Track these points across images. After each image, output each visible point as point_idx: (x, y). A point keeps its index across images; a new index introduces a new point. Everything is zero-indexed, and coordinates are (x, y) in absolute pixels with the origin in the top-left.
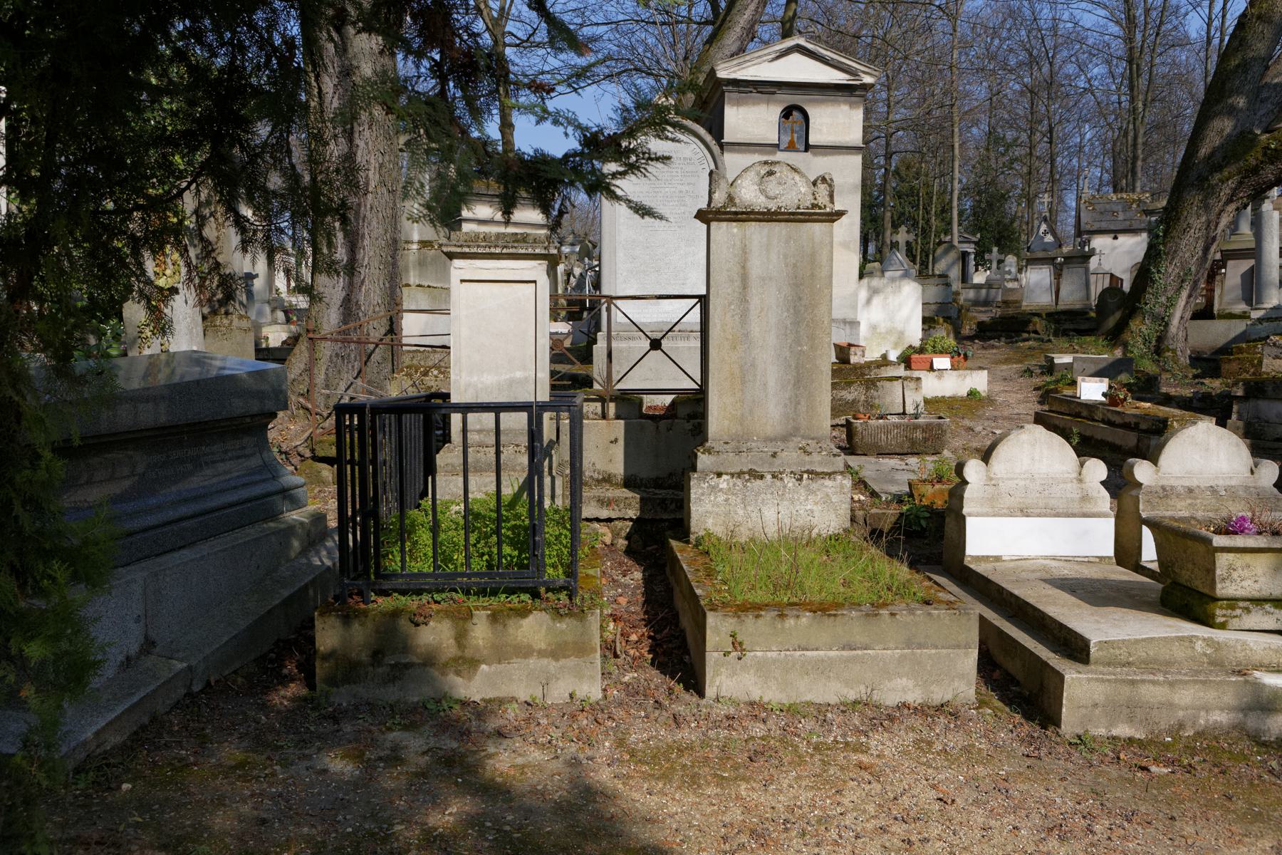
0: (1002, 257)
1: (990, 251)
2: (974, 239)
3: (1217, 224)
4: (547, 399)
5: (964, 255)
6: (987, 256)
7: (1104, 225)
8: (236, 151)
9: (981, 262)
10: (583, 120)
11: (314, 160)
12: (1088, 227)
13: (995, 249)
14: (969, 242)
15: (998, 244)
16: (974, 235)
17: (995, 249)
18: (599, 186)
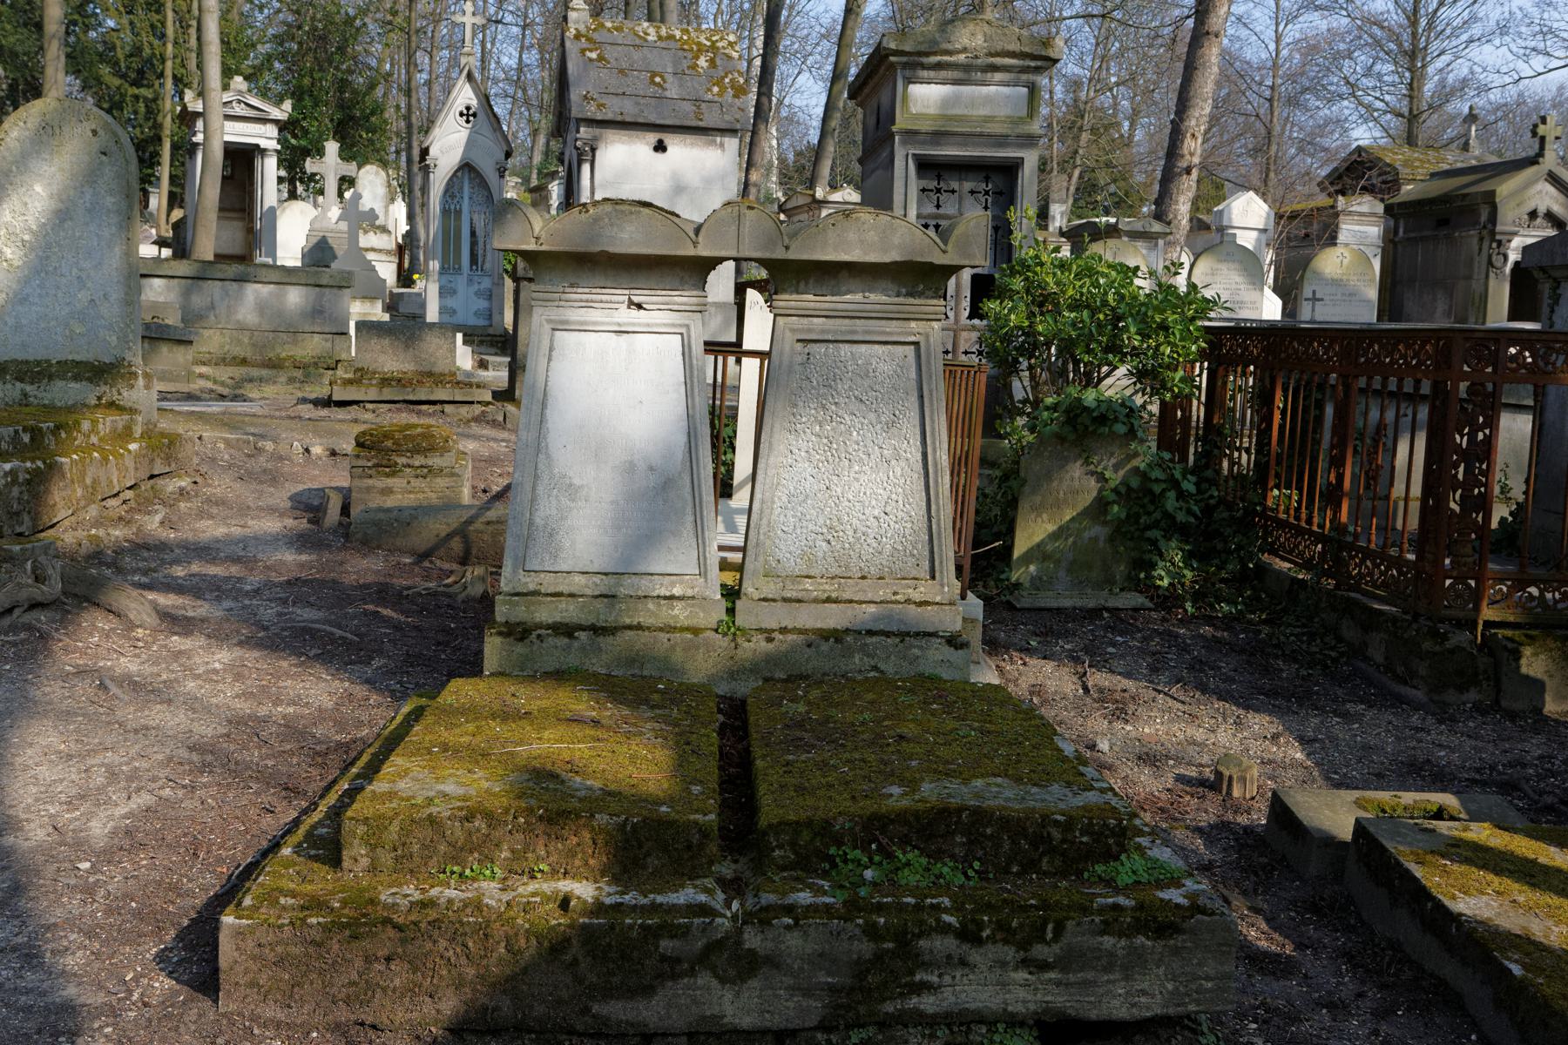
0: (350, 169)
1: (321, 152)
2: (276, 113)
3: (834, 162)
4: (1278, 317)
5: (241, 159)
6: (310, 166)
7: (629, 110)
8: (1409, 456)
9: (297, 181)
10: (745, 585)
11: (293, 894)
12: (591, 111)
13: (332, 147)
14: (264, 121)
15: (342, 132)
16: (278, 102)
17: (332, 147)
18: (354, 103)
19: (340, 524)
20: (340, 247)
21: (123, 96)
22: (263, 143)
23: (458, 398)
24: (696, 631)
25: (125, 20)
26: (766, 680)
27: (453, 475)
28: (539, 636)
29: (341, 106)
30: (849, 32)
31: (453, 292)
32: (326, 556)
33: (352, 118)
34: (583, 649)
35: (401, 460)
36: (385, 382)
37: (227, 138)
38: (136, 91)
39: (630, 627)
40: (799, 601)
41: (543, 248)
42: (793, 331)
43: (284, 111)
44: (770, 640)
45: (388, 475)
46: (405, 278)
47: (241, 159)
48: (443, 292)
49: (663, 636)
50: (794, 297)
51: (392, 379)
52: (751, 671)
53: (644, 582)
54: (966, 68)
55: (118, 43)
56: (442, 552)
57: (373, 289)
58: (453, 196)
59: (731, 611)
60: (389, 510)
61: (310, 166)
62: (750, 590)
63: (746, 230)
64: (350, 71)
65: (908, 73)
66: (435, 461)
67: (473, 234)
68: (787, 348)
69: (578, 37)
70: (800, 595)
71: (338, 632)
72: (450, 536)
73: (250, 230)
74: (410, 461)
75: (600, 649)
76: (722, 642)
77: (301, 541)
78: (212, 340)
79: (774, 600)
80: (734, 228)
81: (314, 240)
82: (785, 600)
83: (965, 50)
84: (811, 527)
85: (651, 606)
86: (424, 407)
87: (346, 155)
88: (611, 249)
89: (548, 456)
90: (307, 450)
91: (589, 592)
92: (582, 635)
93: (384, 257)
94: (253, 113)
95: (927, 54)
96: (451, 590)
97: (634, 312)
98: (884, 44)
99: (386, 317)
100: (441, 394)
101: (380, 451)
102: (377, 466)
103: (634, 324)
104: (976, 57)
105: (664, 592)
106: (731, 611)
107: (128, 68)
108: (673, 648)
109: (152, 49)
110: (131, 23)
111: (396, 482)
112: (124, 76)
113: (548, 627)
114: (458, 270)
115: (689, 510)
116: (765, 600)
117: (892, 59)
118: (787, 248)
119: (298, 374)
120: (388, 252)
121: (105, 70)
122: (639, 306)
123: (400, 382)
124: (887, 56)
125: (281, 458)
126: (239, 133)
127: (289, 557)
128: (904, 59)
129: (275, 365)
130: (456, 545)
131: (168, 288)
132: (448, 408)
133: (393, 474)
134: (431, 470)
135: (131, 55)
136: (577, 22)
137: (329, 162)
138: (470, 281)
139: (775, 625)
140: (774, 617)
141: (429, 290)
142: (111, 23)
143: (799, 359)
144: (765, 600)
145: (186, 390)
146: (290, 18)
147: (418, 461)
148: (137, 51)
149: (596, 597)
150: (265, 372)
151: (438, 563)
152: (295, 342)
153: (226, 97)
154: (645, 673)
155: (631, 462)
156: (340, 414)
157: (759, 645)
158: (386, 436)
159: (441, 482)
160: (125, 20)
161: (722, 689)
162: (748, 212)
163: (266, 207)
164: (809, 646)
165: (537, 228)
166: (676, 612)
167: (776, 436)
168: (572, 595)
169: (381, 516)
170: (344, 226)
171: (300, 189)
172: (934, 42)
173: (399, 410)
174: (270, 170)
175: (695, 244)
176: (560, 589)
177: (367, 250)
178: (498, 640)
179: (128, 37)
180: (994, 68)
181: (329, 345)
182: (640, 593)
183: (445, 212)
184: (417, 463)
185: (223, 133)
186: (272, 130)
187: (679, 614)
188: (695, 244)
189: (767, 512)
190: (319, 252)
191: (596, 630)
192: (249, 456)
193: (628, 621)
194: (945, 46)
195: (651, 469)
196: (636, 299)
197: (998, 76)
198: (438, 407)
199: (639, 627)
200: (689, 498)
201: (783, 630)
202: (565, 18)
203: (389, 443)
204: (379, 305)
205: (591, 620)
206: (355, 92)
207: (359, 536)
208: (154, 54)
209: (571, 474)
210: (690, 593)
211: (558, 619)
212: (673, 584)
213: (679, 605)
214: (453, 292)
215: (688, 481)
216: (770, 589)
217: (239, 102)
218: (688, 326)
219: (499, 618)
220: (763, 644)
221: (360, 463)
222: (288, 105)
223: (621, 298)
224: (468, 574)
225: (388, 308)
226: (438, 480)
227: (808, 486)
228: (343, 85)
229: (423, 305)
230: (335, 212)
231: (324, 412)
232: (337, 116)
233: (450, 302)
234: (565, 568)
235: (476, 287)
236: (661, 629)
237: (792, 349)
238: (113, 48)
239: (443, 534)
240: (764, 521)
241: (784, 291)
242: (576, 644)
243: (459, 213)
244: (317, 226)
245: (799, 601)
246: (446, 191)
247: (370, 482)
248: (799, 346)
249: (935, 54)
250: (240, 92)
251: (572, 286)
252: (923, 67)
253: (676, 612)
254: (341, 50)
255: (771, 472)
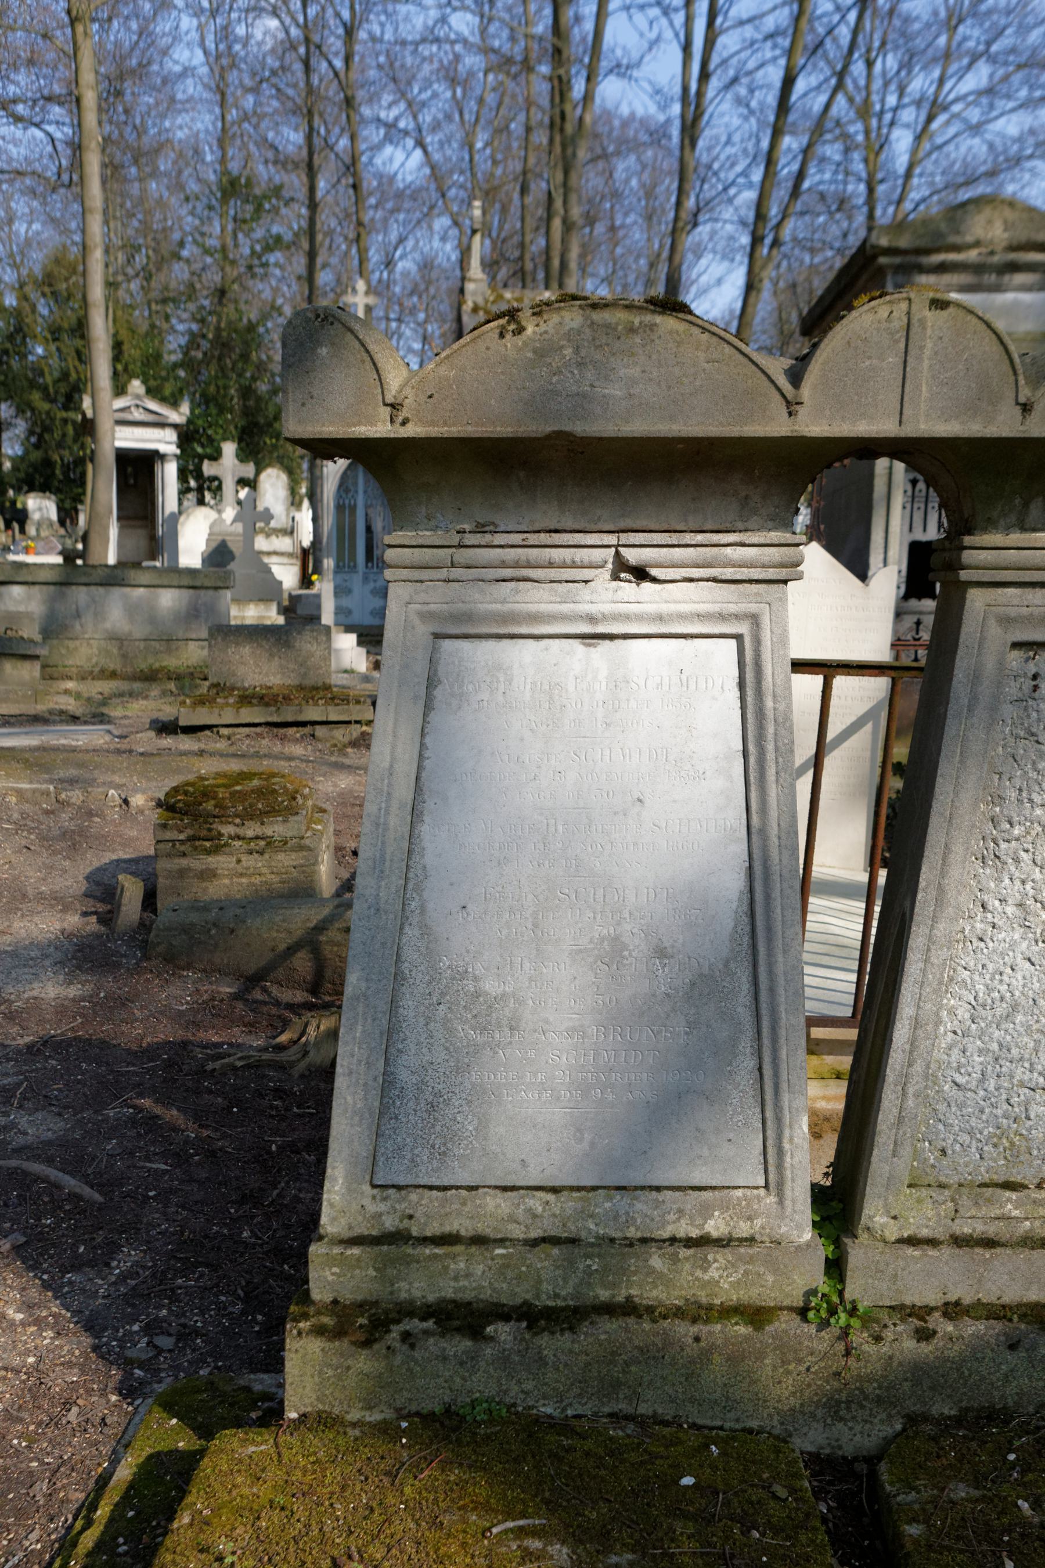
6: (208, 469)
9: (200, 487)
13: (229, 449)
14: (162, 425)
16: (174, 404)
17: (229, 449)
19: (142, 924)
20: (236, 547)
21: (53, 419)
22: (163, 448)
23: (333, 717)
24: (757, 1315)
25: (53, 347)
26: (912, 1420)
27: (301, 848)
28: (406, 1336)
29: (246, 412)
30: (749, 310)
31: (349, 591)
32: (109, 983)
33: (256, 424)
34: (504, 1361)
35: (227, 830)
36: (247, 698)
37: (119, 444)
38: (64, 414)
39: (609, 1309)
40: (989, 1243)
41: (411, 431)
42: (1006, 621)
43: (179, 415)
44: (924, 1335)
45: (208, 852)
46: (306, 581)
47: (136, 468)
48: (340, 592)
49: (684, 1330)
50: (1016, 538)
51: (253, 696)
52: (879, 1400)
53: (642, 1205)
54: (978, 269)
55: (46, 370)
56: (280, 973)
57: (267, 589)
58: (347, 491)
59: (836, 1267)
60: (206, 908)
61: (208, 469)
62: (880, 1220)
63: (923, 366)
64: (254, 379)
65: (900, 278)
66: (276, 829)
67: (369, 529)
68: (990, 664)
69: (475, 309)
70: (991, 1230)
71: (70, 1183)
72: (292, 950)
73: (153, 538)
74: (240, 831)
75: (542, 1361)
76: (816, 1341)
77: (82, 956)
78: (85, 649)
79: (932, 1242)
80: (893, 360)
81: (214, 545)
82: (959, 1241)
83: (977, 244)
84: (1020, 1074)
85: (656, 1262)
86: (291, 731)
87: (243, 456)
88: (581, 428)
89: (426, 930)
90: (126, 801)
91: (517, 1232)
92: (503, 1331)
93: (285, 560)
94: (150, 418)
95: (928, 252)
96: (283, 1057)
97: (628, 589)
98: (874, 239)
99: (281, 620)
100: (313, 713)
101: (196, 817)
102: (192, 839)
103: (627, 618)
104: (992, 253)
105: (685, 1229)
106: (836, 1267)
107: (56, 392)
108: (706, 1355)
109: (78, 372)
110: (58, 349)
111: (221, 862)
112: (53, 401)
113: (428, 1311)
114: (354, 568)
115: (746, 1044)
116: (912, 1241)
117: (883, 260)
118: (1026, 408)
119: (172, 686)
120: (290, 555)
121: (36, 397)
122: (641, 574)
123: (263, 698)
124: (874, 257)
125: (90, 814)
126: (129, 439)
127: (52, 989)
128: (897, 260)
129: (150, 677)
130: (302, 963)
131: (29, 598)
132: (320, 731)
133: (216, 850)
134: (269, 841)
135: (59, 380)
136: (474, 293)
137: (228, 462)
138: (366, 579)
139: (933, 1298)
140: (933, 1278)
141: (325, 588)
142: (40, 351)
143: (1012, 689)
144: (912, 1241)
145: (32, 712)
146: (194, 327)
147: (251, 830)
148: (65, 375)
149: (534, 1243)
150: (137, 686)
151: (275, 990)
152: (169, 651)
153: (120, 403)
154: (644, 1409)
155: (616, 938)
156: (186, 743)
157: (902, 1343)
158: (207, 794)
159: (285, 860)
160: (53, 347)
161: (811, 1439)
162: (932, 317)
163: (167, 512)
164: (1013, 1347)
165: (395, 380)
166: (713, 1273)
167: (955, 872)
168: (479, 1241)
169: (194, 917)
170: (239, 527)
171: (208, 496)
172: (939, 235)
173: (260, 735)
174: (170, 472)
175: (792, 406)
176: (453, 1226)
177: (269, 554)
178: (315, 1346)
179: (54, 362)
180: (1014, 267)
181: (205, 652)
182: (632, 1233)
183: (340, 508)
184: (250, 833)
185: (114, 439)
186: (171, 435)
187: (722, 1278)
188: (792, 406)
189: (923, 1044)
190: (219, 555)
191: (534, 1317)
192: (47, 812)
193: (604, 1295)
194: (953, 239)
195: (661, 953)
196: (632, 556)
197: (1020, 278)
198: (308, 730)
199: (629, 1309)
200: (745, 1015)
201: (953, 1310)
202: (462, 291)
203: (209, 806)
204: (274, 608)
205: (523, 1293)
206: (259, 399)
207: (160, 949)
208: (79, 379)
209: (479, 970)
210: (744, 1229)
211: (449, 1294)
212: (706, 1210)
213: (719, 1258)
214: (349, 591)
215: (746, 986)
216: (925, 1216)
217: (137, 406)
218: (754, 619)
219: (319, 1293)
220: (909, 1344)
221: (169, 835)
222: (185, 408)
223: (597, 555)
224: (311, 1031)
225: (284, 611)
226: (281, 856)
227: (1018, 982)
228: (247, 392)
229: (319, 607)
230: (230, 513)
231: (168, 741)
232: (242, 423)
233: (346, 602)
234: (464, 1178)
235: (372, 585)
236: (678, 1313)
237: (1001, 663)
238: (42, 374)
239: (282, 947)
240: (918, 1067)
241: (990, 525)
242: (489, 1351)
243: (353, 509)
244: (216, 529)
245: (989, 1243)
246: (340, 486)
247: (184, 862)
248: (1015, 658)
249: (938, 250)
250: (138, 397)
251: (480, 529)
252: (922, 269)
253: (713, 1273)
254: (245, 357)
255: (938, 956)
